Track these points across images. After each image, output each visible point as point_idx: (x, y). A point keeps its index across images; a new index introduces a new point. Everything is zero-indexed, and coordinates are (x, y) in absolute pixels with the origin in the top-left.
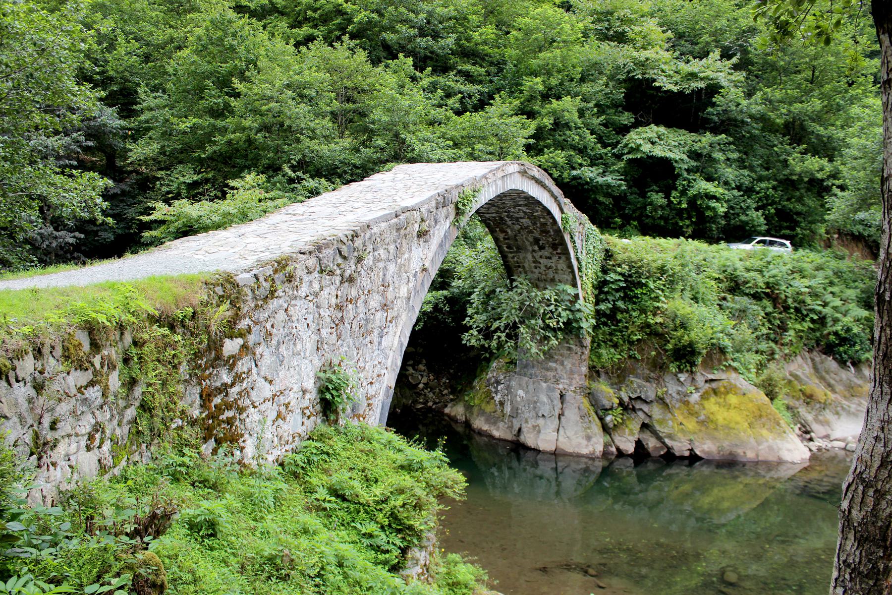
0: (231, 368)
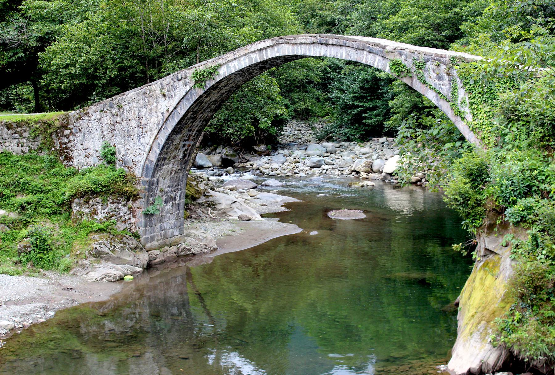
0: (68, 138)
